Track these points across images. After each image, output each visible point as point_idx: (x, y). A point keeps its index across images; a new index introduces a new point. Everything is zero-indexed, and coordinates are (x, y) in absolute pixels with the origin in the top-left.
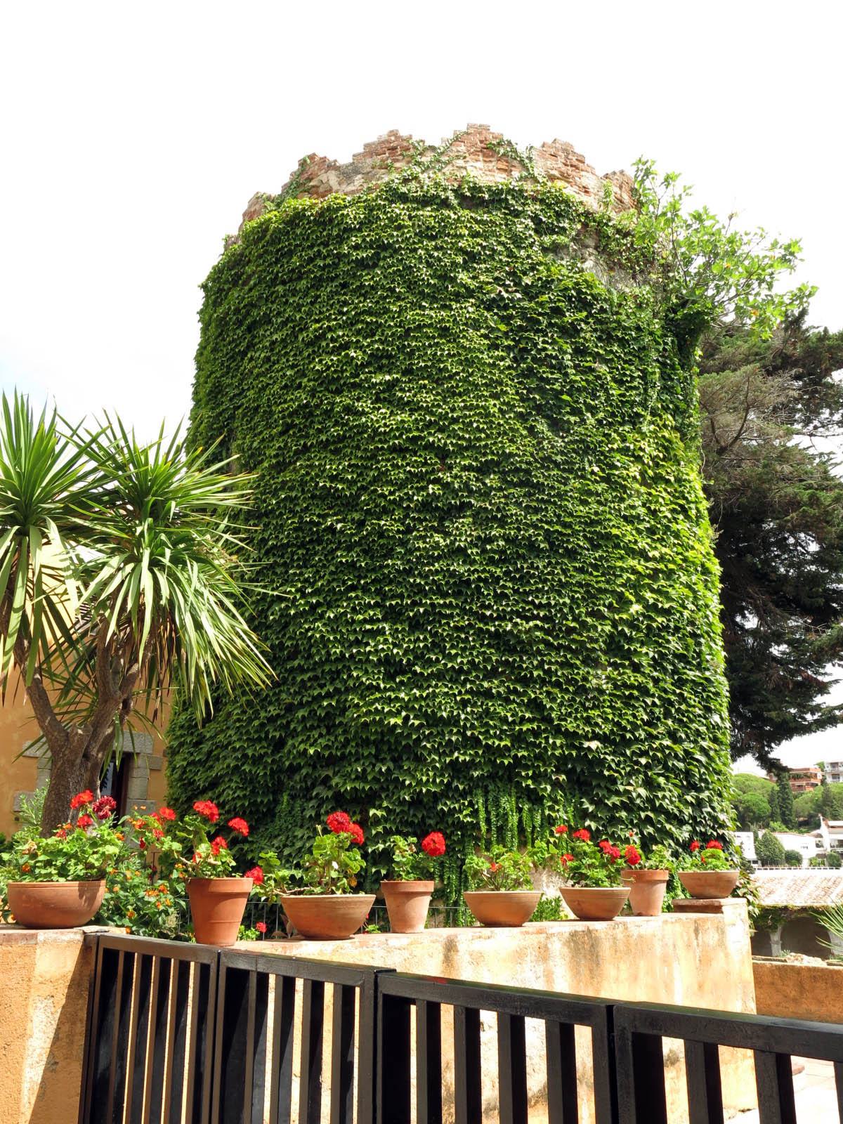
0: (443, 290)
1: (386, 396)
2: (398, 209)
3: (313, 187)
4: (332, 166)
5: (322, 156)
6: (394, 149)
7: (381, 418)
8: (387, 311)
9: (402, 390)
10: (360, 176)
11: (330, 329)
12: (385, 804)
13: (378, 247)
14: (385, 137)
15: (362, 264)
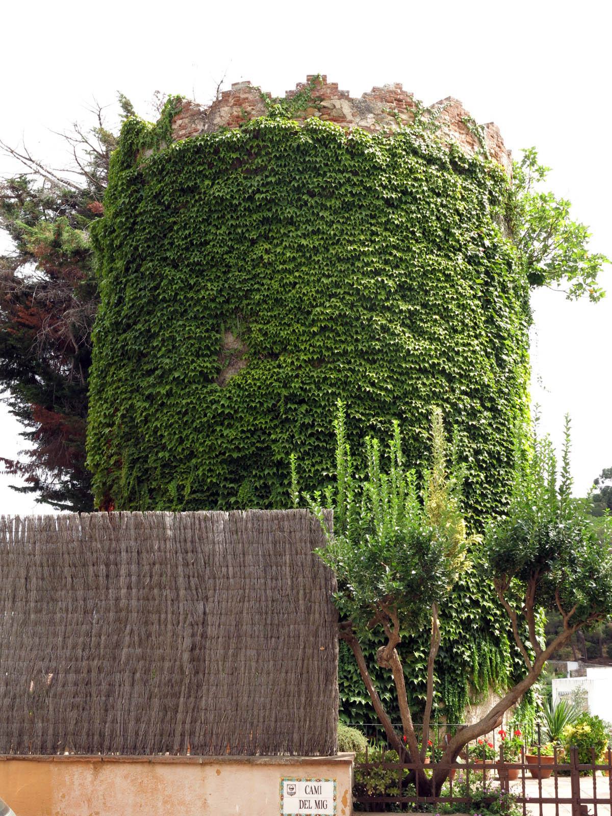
0: (445, 244)
1: (412, 323)
2: (412, 160)
3: (324, 107)
4: (344, 96)
5: (176, 95)
6: (399, 101)
7: (414, 345)
8: (409, 249)
9: (421, 320)
10: (371, 115)
11: (364, 253)
12: (422, 649)
13: (402, 192)
14: (392, 88)
15: (389, 202)
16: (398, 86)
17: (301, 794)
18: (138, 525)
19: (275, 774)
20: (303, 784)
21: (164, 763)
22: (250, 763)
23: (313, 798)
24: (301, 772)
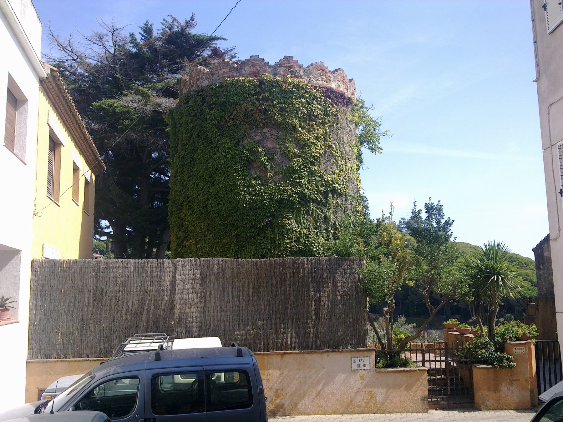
4: (301, 67)
16: (322, 63)
17: (358, 362)
18: (294, 263)
19: (348, 355)
20: (359, 358)
21: (308, 353)
22: (550, 259)
23: (362, 363)
24: (358, 354)
